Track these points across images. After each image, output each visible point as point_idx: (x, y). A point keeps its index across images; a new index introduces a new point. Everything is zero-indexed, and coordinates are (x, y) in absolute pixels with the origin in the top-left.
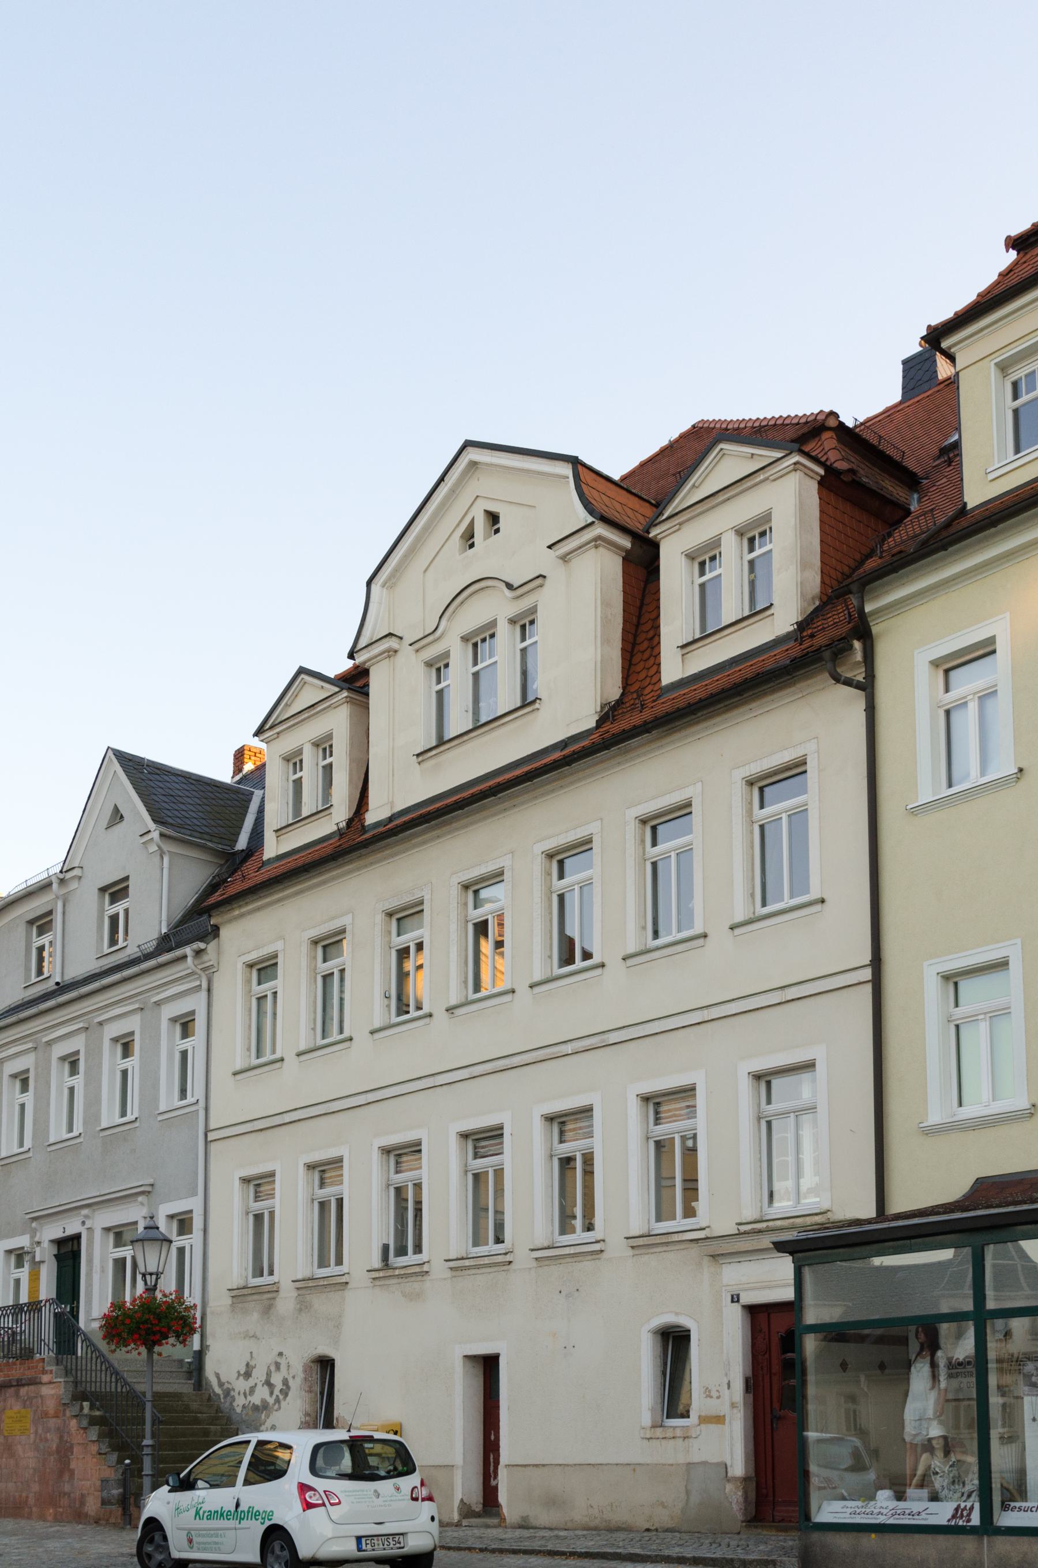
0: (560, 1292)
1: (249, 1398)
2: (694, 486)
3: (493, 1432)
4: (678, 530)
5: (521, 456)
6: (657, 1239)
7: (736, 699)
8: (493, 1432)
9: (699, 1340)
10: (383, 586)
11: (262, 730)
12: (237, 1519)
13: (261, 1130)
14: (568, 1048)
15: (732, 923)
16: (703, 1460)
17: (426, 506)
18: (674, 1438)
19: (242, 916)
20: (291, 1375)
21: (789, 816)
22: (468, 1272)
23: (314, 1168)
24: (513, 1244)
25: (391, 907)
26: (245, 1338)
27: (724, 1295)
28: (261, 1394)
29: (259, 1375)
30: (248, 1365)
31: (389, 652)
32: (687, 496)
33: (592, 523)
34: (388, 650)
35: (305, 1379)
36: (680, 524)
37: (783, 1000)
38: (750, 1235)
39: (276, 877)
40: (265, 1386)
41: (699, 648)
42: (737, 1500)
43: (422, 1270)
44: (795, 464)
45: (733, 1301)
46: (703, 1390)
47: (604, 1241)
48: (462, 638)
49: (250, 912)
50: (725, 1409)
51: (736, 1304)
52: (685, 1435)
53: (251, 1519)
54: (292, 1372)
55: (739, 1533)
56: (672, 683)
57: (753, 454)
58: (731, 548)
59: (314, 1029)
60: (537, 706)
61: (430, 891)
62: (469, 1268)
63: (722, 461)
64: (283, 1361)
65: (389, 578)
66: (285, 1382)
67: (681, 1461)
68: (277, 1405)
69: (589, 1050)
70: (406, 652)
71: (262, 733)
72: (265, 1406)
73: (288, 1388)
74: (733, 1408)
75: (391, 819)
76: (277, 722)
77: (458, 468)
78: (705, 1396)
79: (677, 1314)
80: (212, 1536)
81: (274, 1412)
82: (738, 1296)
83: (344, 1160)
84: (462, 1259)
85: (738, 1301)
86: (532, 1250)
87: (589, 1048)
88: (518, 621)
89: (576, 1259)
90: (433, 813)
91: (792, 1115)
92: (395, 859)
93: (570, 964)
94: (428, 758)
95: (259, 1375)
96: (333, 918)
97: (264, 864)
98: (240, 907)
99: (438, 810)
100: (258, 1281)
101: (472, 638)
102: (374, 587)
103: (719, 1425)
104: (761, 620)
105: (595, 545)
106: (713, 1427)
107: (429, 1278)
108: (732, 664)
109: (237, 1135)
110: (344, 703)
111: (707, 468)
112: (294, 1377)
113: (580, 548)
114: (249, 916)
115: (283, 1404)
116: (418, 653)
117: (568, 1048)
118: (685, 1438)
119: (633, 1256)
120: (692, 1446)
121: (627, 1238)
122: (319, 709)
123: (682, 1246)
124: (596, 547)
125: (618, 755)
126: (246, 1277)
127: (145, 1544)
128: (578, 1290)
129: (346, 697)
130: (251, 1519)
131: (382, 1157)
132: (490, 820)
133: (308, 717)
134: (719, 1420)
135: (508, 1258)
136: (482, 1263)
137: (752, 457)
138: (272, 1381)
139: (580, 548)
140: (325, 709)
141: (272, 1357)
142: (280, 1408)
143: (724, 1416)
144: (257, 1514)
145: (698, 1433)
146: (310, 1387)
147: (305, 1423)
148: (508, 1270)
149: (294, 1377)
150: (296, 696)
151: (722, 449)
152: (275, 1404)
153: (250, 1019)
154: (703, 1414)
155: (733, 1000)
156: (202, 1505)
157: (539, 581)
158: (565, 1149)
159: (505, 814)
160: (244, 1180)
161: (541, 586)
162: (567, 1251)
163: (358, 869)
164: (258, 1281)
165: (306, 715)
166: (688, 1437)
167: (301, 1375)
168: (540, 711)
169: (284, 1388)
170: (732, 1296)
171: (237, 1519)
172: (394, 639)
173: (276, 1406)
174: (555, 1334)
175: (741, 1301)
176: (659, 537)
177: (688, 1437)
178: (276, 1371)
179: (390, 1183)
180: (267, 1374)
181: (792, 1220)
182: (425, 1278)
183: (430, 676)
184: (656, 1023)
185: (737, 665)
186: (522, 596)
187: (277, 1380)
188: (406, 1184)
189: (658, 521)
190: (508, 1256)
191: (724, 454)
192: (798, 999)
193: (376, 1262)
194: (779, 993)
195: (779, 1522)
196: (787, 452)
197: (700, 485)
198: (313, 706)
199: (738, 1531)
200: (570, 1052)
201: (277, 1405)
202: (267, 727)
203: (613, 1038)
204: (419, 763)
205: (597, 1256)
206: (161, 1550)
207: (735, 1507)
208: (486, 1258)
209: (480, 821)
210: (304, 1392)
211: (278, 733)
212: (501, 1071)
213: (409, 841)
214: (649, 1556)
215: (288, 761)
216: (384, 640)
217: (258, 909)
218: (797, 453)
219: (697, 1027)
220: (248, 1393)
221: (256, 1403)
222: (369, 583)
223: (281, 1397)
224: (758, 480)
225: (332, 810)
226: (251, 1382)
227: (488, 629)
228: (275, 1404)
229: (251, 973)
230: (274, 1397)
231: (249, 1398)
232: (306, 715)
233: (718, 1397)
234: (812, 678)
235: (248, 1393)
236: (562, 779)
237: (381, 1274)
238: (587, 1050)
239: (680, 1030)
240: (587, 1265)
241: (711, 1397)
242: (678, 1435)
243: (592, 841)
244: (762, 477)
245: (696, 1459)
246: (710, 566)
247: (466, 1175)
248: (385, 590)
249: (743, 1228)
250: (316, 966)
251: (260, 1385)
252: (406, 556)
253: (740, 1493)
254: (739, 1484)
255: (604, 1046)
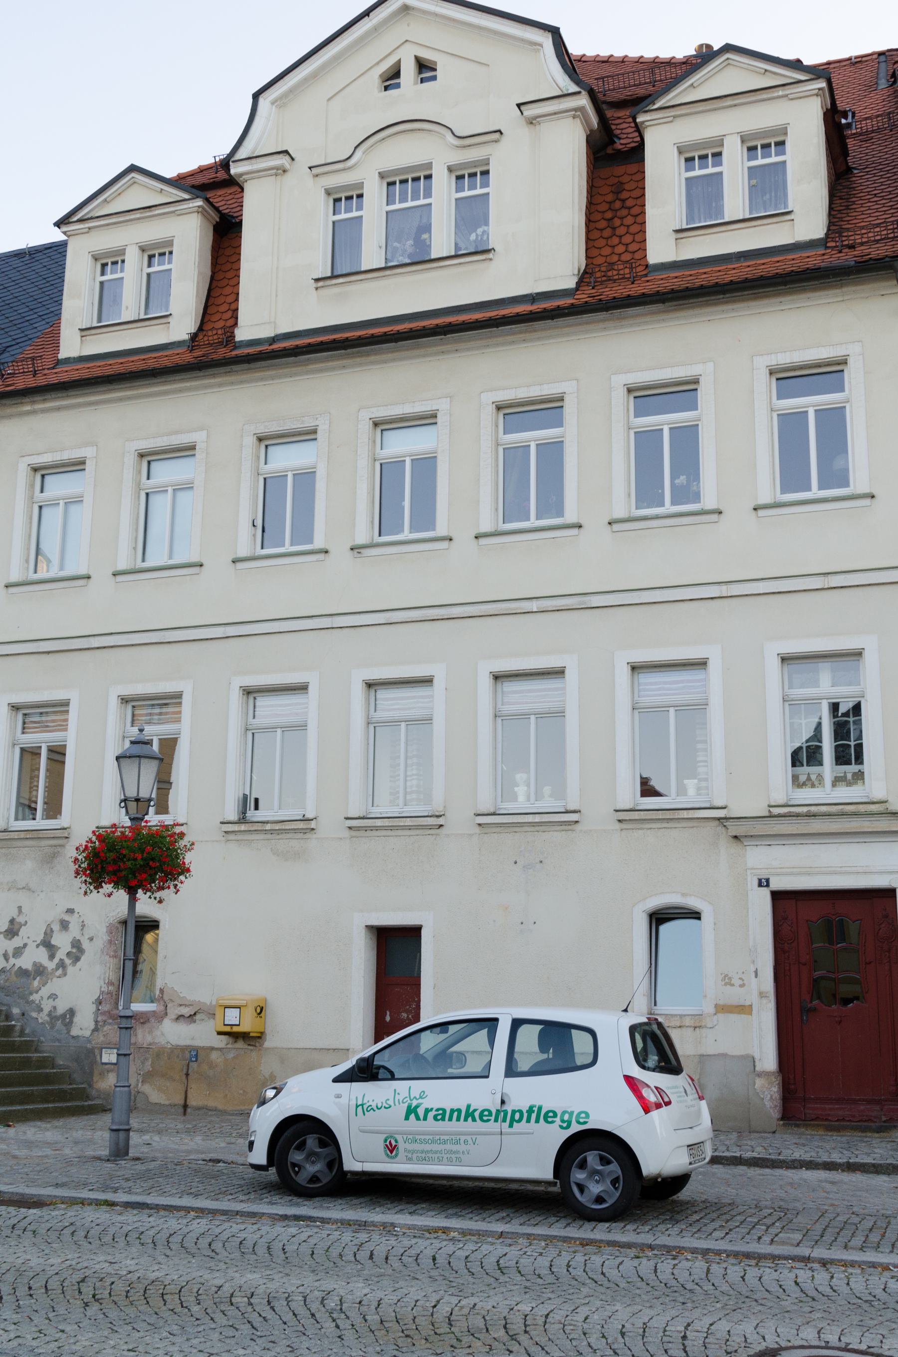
0: (516, 863)
1: (12, 961)
2: (105, 200)
3: (388, 1013)
4: (671, 122)
5: (480, 13)
6: (643, 815)
7: (781, 288)
8: (388, 1013)
9: (715, 924)
10: (273, 103)
11: (66, 221)
12: (504, 1120)
13: (48, 653)
14: (534, 606)
15: (235, 557)
16: (721, 1052)
17: (342, 35)
18: (680, 1027)
19: (34, 412)
20: (87, 937)
21: (65, 503)
22: (375, 833)
23: (18, 709)
24: (445, 807)
25: (267, 431)
26: (9, 890)
27: (749, 879)
28: (34, 956)
29: (32, 933)
30: (12, 921)
31: (277, 170)
32: (680, 94)
33: (579, 93)
34: (277, 168)
35: (110, 942)
36: (674, 117)
37: (826, 587)
38: (799, 818)
39: (108, 376)
40: (41, 947)
41: (768, 224)
42: (771, 1096)
43: (309, 827)
44: (819, 89)
45: (760, 885)
46: (721, 977)
47: (186, 824)
48: (379, 173)
49: (43, 411)
50: (752, 998)
51: (766, 888)
52: (698, 1025)
53: (537, 1121)
54: (88, 933)
55: (774, 1132)
56: (662, 263)
57: (766, 70)
58: (133, 258)
59: (135, 549)
60: (491, 256)
61: (328, 422)
62: (377, 828)
63: (725, 69)
64: (73, 920)
65: (280, 98)
66: (76, 944)
67: (692, 1053)
68: (61, 970)
69: (562, 610)
70: (299, 172)
71: (66, 224)
72: (39, 971)
73: (81, 951)
74: (762, 997)
75: (273, 340)
76: (86, 217)
77: (388, 8)
78: (723, 983)
79: (684, 895)
80: (445, 1142)
81: (55, 979)
82: (768, 880)
83: (184, 696)
84: (363, 818)
85: (768, 885)
86: (347, 818)
87: (563, 608)
88: (456, 170)
89: (537, 828)
90: (414, 331)
91: (403, 724)
92: (275, 382)
93: (660, 507)
94: (332, 285)
95: (32, 933)
96: (176, 433)
97: (59, 362)
98: (34, 402)
99: (464, 323)
100: (28, 824)
101: (388, 177)
102: (264, 102)
103: (743, 1016)
104: (777, 223)
105: (574, 115)
106: (735, 1018)
107: (315, 836)
108: (740, 257)
109: (80, 650)
110: (194, 212)
111: (708, 72)
112: (91, 939)
113: (555, 114)
114: (41, 415)
115: (70, 970)
116: (317, 179)
117: (534, 606)
118: (695, 1028)
119: (622, 830)
120: (706, 1037)
121: (617, 811)
122: (157, 212)
123: (690, 824)
124: (574, 117)
125: (611, 320)
126: (8, 819)
127: (291, 1150)
128: (541, 862)
129: (199, 207)
130: (537, 1121)
131: (121, 707)
132: (418, 361)
133: (139, 219)
134: (744, 1009)
135: (441, 821)
136: (402, 824)
137: (161, 192)
138: (53, 942)
139: (555, 114)
140: (164, 214)
141: (58, 912)
142: (65, 975)
143: (751, 1006)
144: (517, 1116)
145: (715, 1023)
146: (115, 951)
147: (108, 993)
148: (436, 835)
149: (91, 939)
150: (119, 194)
151: (728, 59)
152: (57, 969)
153: (30, 528)
154: (721, 1002)
155: (762, 579)
156: (420, 1101)
157: (497, 135)
158: (31, 739)
159: (440, 357)
160: (13, 707)
161: (496, 142)
162: (379, 823)
163: (220, 385)
164: (28, 824)
165: (138, 216)
166: (700, 1027)
167: (102, 937)
168: (493, 262)
169: (74, 950)
170: (760, 881)
171: (504, 1120)
172: (287, 157)
173: (60, 972)
174: (506, 908)
175: (771, 885)
176: (647, 123)
177: (700, 1027)
178: (61, 930)
179: (250, 727)
180: (45, 933)
181: (841, 807)
182: (308, 836)
183: (328, 205)
184: (658, 592)
185: (745, 260)
186: (469, 146)
187: (62, 941)
188: (151, 738)
189: (647, 109)
190: (441, 819)
191: (729, 64)
192: (211, 639)
193: (232, 814)
194: (822, 578)
195: (812, 1120)
196: (813, 77)
197: (111, 201)
198: (149, 207)
199: (774, 1130)
200: (535, 610)
201: (61, 970)
202: (75, 219)
203: (596, 601)
204: (317, 289)
205: (570, 827)
206: (597, 1177)
207: (768, 1104)
208: (408, 819)
209: (286, 376)
210: (107, 957)
211: (89, 228)
212: (433, 620)
213: (305, 365)
214: (784, 1161)
215: (96, 260)
216: (275, 156)
217: (58, 409)
218: (824, 80)
219: (710, 601)
220: (11, 955)
221: (24, 967)
222: (256, 96)
223: (68, 961)
224: (776, 94)
225: (170, 319)
226: (17, 942)
227: (413, 172)
228: (57, 969)
229: (34, 477)
230: (56, 960)
231: (12, 961)
232: (138, 216)
233: (742, 986)
234: (862, 285)
235: (11, 955)
236: (531, 332)
237: (235, 828)
238: (558, 610)
239: (686, 602)
240: (556, 836)
241: (733, 985)
242: (687, 1024)
243: (316, 432)
244: (781, 93)
245: (710, 1051)
246: (159, 260)
247: (368, 727)
248: (274, 107)
249: (776, 811)
250: (140, 481)
251: (32, 946)
252: (314, 76)
253: (775, 1089)
254: (774, 1080)
255: (582, 608)
